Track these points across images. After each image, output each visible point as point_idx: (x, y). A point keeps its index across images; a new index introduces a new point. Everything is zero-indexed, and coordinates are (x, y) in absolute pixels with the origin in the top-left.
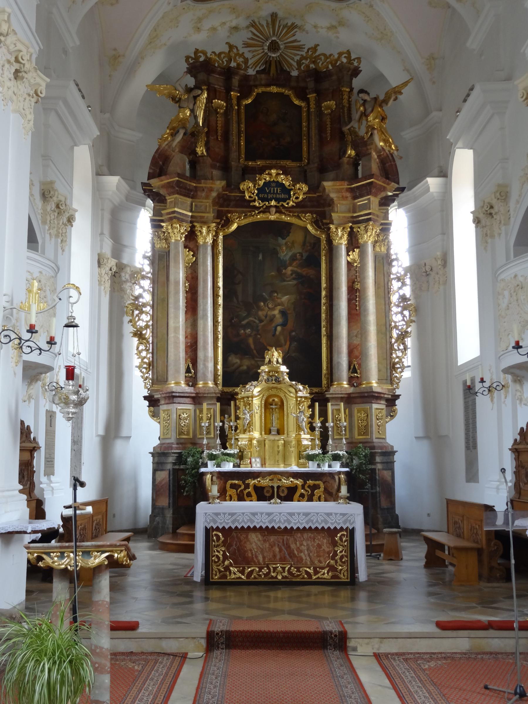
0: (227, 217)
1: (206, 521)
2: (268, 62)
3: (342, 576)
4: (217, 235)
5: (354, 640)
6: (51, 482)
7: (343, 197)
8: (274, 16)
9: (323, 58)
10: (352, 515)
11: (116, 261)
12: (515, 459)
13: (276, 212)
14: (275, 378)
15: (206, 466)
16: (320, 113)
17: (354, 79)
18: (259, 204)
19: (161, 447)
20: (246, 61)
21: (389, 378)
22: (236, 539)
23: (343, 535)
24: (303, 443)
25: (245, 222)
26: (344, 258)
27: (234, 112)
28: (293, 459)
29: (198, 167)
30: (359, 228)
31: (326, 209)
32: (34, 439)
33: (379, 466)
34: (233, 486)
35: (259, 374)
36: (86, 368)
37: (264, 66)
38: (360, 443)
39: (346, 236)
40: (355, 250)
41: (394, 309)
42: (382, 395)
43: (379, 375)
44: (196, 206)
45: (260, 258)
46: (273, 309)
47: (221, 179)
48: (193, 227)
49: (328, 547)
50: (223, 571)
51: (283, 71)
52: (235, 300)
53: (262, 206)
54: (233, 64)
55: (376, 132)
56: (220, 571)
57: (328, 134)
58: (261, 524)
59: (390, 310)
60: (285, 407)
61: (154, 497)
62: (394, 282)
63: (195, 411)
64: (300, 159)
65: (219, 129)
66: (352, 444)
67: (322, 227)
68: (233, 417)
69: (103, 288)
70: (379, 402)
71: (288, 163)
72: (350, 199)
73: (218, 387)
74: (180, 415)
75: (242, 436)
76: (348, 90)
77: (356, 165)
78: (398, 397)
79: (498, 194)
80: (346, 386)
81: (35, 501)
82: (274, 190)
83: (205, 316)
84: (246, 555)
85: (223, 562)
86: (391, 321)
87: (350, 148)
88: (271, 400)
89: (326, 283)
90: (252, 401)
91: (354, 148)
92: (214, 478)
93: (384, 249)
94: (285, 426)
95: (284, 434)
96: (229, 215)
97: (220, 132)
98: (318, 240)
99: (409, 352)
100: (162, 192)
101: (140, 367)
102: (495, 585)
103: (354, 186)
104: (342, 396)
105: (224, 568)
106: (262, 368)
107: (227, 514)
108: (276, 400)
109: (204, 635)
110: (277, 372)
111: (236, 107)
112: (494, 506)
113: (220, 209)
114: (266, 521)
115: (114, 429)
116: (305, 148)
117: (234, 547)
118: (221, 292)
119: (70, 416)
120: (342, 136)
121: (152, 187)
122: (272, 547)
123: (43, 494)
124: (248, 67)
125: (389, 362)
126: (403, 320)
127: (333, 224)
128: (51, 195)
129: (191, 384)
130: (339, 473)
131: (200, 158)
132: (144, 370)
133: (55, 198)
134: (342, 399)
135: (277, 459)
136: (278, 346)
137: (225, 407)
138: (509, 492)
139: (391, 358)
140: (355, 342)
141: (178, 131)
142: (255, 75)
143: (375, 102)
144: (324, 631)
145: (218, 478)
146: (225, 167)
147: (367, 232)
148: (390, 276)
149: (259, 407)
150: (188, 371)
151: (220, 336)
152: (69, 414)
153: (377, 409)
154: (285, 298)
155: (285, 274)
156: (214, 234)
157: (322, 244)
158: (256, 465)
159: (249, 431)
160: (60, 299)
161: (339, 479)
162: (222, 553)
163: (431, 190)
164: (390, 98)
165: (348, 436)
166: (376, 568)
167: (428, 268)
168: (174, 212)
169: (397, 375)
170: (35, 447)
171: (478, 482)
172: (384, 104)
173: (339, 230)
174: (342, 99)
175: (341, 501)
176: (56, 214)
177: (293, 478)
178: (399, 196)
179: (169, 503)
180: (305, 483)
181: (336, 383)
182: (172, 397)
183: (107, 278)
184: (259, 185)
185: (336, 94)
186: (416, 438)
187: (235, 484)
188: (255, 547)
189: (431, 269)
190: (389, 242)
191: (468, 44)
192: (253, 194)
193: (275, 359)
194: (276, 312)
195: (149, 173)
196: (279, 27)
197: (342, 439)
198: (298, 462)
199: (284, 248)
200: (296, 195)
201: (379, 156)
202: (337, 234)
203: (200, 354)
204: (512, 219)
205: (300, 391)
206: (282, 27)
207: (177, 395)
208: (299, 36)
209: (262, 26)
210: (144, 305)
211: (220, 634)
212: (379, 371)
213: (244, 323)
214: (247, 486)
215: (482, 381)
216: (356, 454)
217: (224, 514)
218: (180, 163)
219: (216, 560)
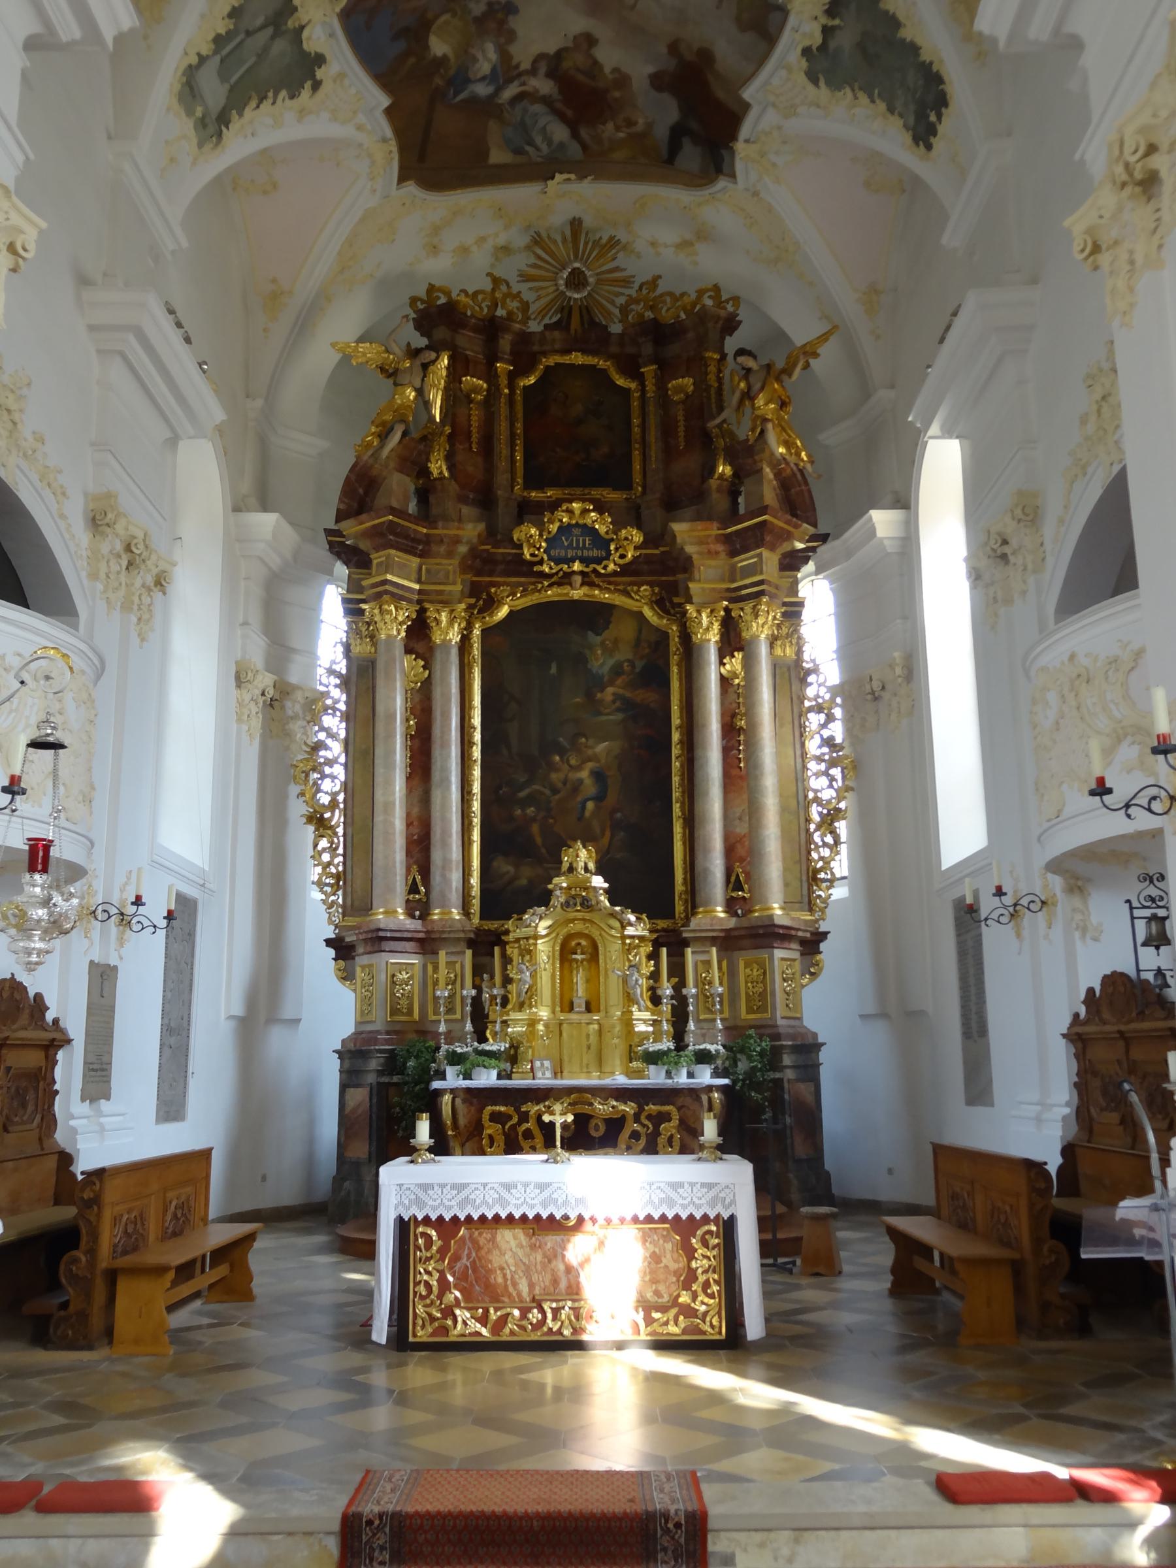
1: (401, 1203)
2: (567, 310)
3: (707, 1328)
4: (469, 627)
5: (728, 1534)
6: (100, 1114)
7: (709, 552)
8: (576, 224)
9: (668, 299)
10: (727, 1187)
11: (275, 678)
12: (1076, 1056)
13: (583, 584)
14: (583, 901)
15: (442, 1076)
17: (727, 338)
18: (551, 568)
19: (356, 1039)
20: (525, 306)
21: (806, 900)
22: (469, 1244)
23: (710, 1232)
24: (637, 1029)
25: (522, 602)
26: (713, 667)
27: (503, 400)
28: (618, 1062)
29: (432, 499)
30: (742, 609)
31: (680, 577)
32: (56, 1021)
33: (789, 1074)
34: (496, 1118)
35: (550, 893)
36: (202, 882)
37: (559, 316)
38: (751, 1027)
39: (716, 626)
40: (736, 654)
41: (813, 766)
42: (793, 933)
43: (786, 894)
44: (428, 571)
46: (579, 768)
47: (479, 520)
48: (422, 612)
49: (675, 1261)
50: (438, 1319)
51: (593, 324)
52: (505, 751)
53: (557, 573)
54: (500, 312)
55: (770, 426)
56: (433, 1319)
57: (681, 439)
58: (524, 1209)
59: (805, 768)
60: (601, 957)
61: (342, 1139)
62: (812, 716)
63: (425, 967)
64: (628, 486)
65: (474, 430)
66: (734, 1030)
67: (672, 611)
68: (498, 978)
69: (245, 728)
70: (786, 945)
71: (604, 493)
72: (723, 555)
73: (470, 919)
74: (393, 976)
75: (514, 1015)
76: (717, 356)
77: (734, 494)
78: (824, 935)
79: (1018, 512)
80: (722, 915)
81: (56, 1157)
82: (578, 541)
83: (446, 781)
84: (492, 1281)
85: (440, 1296)
86: (806, 789)
87: (721, 461)
88: (573, 943)
89: (681, 718)
90: (536, 944)
91: (731, 460)
92: (458, 1101)
93: (790, 652)
94: (602, 995)
95: (599, 1011)
96: (493, 590)
97: (475, 437)
98: (664, 636)
99: (843, 848)
100: (364, 545)
101: (320, 884)
102: (1054, 1344)
103: (730, 530)
104: (714, 934)
105: (441, 1311)
106: (556, 880)
107: (532, 1186)
108: (584, 943)
109: (336, 1526)
110: (586, 889)
111: (506, 391)
112: (1046, 1163)
113: (475, 579)
114: (536, 1201)
115: (265, 1003)
116: (637, 466)
117: (464, 1261)
118: (477, 737)
119: (34, 958)
120: (706, 440)
121: (343, 536)
122: (550, 1261)
123: (76, 1140)
124: (529, 318)
125: (804, 868)
126: (831, 786)
127: (691, 603)
128: (107, 520)
129: (417, 913)
130: (709, 1089)
131: (437, 482)
132: (329, 889)
133: (119, 527)
134: (713, 941)
135: (585, 1062)
137: (485, 960)
138: (1064, 1128)
139: (809, 860)
140: (738, 830)
141: (392, 429)
142: (542, 333)
143: (768, 372)
144: (647, 1512)
145: (464, 1101)
146: (485, 500)
147: (756, 616)
148: (803, 703)
149: (548, 957)
150: (413, 889)
151: (477, 821)
152: (30, 954)
153: (783, 959)
154: (601, 748)
155: (601, 701)
156: (463, 625)
157: (672, 644)
158: (544, 1074)
159: (531, 1007)
160: (22, 682)
161: (710, 1100)
162: (436, 1275)
163: (880, 533)
164: (795, 365)
165: (726, 1015)
166: (785, 1296)
167: (876, 685)
168: (386, 582)
169: (821, 893)
170: (54, 1040)
171: (992, 1105)
172: (784, 377)
173: (704, 615)
174: (706, 374)
175: (705, 1154)
176: (124, 563)
177: (617, 1101)
178: (818, 550)
179: (370, 1153)
180: (641, 1109)
181: (701, 910)
182: (378, 940)
183: (254, 709)
184: (550, 532)
185: (695, 364)
186: (861, 1016)
187: (500, 1112)
188: (511, 1261)
189: (883, 688)
190: (799, 638)
191: (945, 240)
192: (539, 549)
193: (582, 864)
194: (584, 774)
195: (338, 510)
196: (586, 244)
197: (714, 1020)
198: (628, 1067)
199: (599, 652)
200: (621, 551)
201: (778, 474)
202: (700, 623)
203: (436, 856)
204: (1050, 560)
205: (631, 924)
206: (590, 244)
207: (389, 935)
208: (622, 260)
209: (555, 242)
210: (330, 763)
211: (377, 1522)
212: (786, 885)
213: (522, 794)
214: (524, 1117)
215: (999, 892)
216: (742, 1050)
217: (442, 1186)
218: (399, 489)
219: (424, 1293)
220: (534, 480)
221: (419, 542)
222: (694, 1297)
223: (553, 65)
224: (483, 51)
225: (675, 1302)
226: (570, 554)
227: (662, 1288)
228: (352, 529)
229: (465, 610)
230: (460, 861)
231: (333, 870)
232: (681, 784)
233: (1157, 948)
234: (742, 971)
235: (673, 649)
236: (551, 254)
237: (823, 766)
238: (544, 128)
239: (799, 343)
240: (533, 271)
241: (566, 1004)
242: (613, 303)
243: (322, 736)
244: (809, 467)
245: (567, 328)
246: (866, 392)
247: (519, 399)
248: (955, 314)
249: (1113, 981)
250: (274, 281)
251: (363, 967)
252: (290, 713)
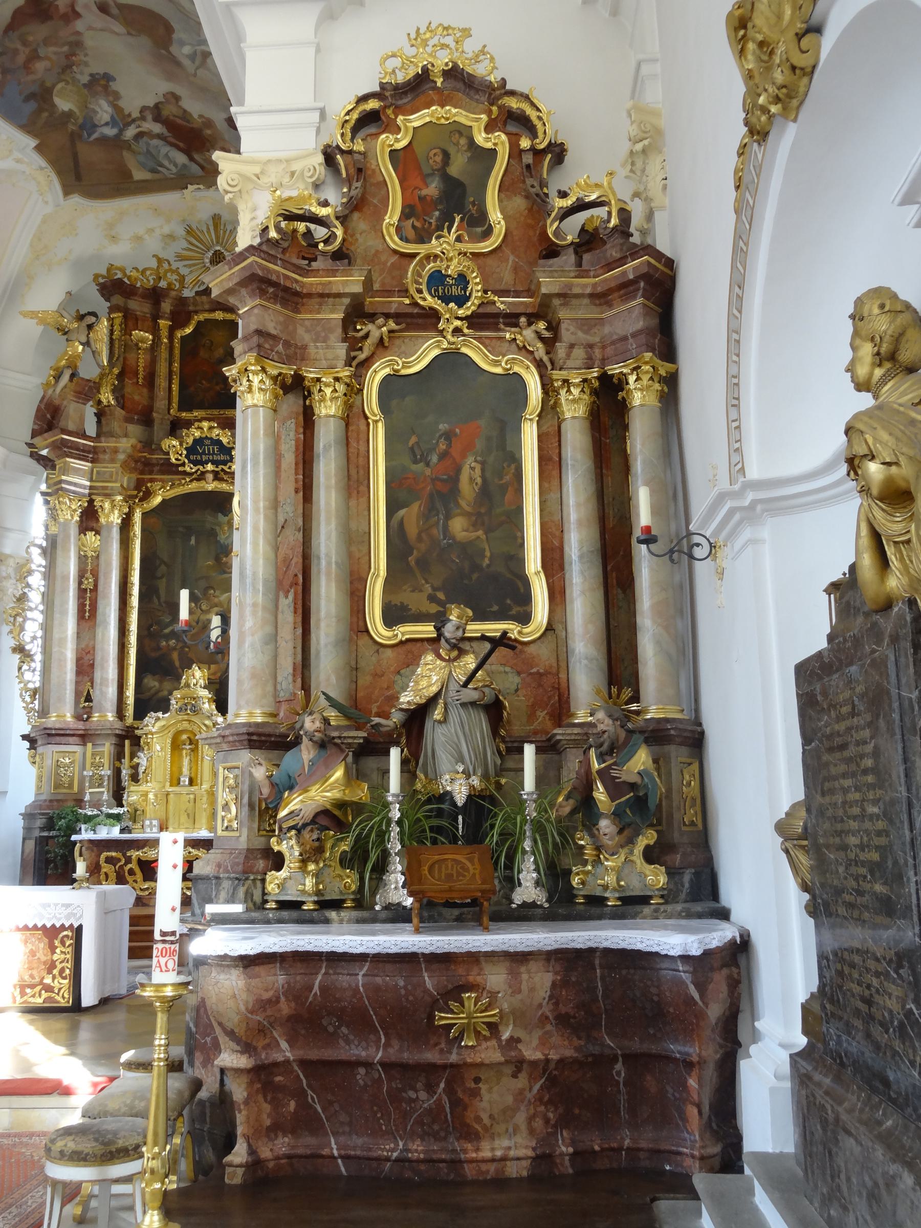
0: (147, 488)
3: (59, 998)
20: (182, 279)
25: (172, 493)
34: (109, 860)
44: (98, 472)
45: (193, 542)
48: (91, 502)
52: (155, 600)
54: (163, 284)
65: (141, 369)
111: (165, 340)
146: (146, 418)
213: (167, 631)
214: (129, 860)
222: (54, 978)
223: (156, 112)
224: (100, 106)
225: (41, 983)
226: (204, 458)
227: (35, 972)
236: (201, 241)
238: (167, 155)
241: (175, 782)
247: (177, 345)
252: (4, 574)
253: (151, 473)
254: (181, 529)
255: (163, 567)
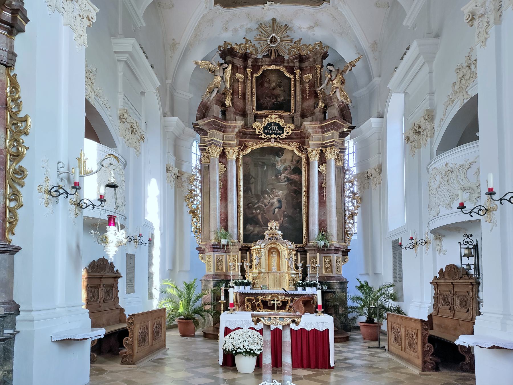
0: (245, 145)
2: (270, 51)
4: (239, 154)
8: (274, 20)
12: (435, 289)
14: (273, 238)
16: (302, 82)
25: (255, 147)
31: (306, 140)
32: (117, 271)
39: (318, 155)
45: (265, 168)
46: (273, 198)
48: (224, 149)
51: (279, 55)
52: (250, 193)
54: (248, 51)
63: (226, 256)
64: (290, 110)
65: (240, 91)
72: (320, 132)
77: (325, 113)
78: (349, 250)
91: (324, 101)
97: (240, 93)
100: (205, 128)
106: (266, 232)
120: (316, 95)
136: (276, 220)
146: (244, 115)
147: (331, 152)
151: (242, 214)
154: (280, 193)
172: (343, 73)
174: (317, 72)
185: (313, 69)
194: (275, 200)
204: (436, 134)
210: (196, 195)
214: (257, 300)
218: (216, 110)
220: (259, 107)
221: (223, 127)
226: (271, 132)
228: (201, 122)
229: (238, 149)
230: (236, 224)
231: (198, 227)
232: (305, 204)
233: (468, 257)
234: (324, 260)
235: (303, 162)
237: (350, 200)
239: (348, 62)
240: (259, 37)
242: (286, 48)
243: (193, 187)
244: (350, 104)
245: (270, 57)
246: (370, 79)
248: (408, 49)
249: (449, 267)
250: (173, 39)
251: (208, 256)
253: (246, 138)
254: (260, 163)
255: (253, 179)
